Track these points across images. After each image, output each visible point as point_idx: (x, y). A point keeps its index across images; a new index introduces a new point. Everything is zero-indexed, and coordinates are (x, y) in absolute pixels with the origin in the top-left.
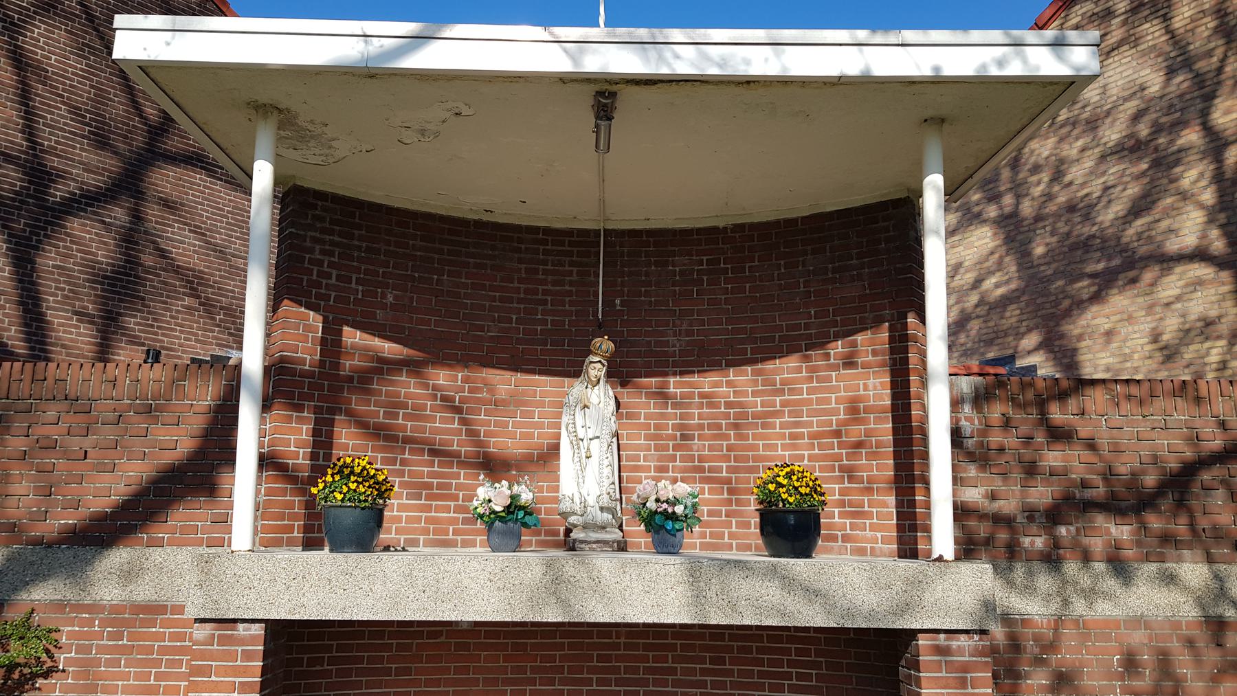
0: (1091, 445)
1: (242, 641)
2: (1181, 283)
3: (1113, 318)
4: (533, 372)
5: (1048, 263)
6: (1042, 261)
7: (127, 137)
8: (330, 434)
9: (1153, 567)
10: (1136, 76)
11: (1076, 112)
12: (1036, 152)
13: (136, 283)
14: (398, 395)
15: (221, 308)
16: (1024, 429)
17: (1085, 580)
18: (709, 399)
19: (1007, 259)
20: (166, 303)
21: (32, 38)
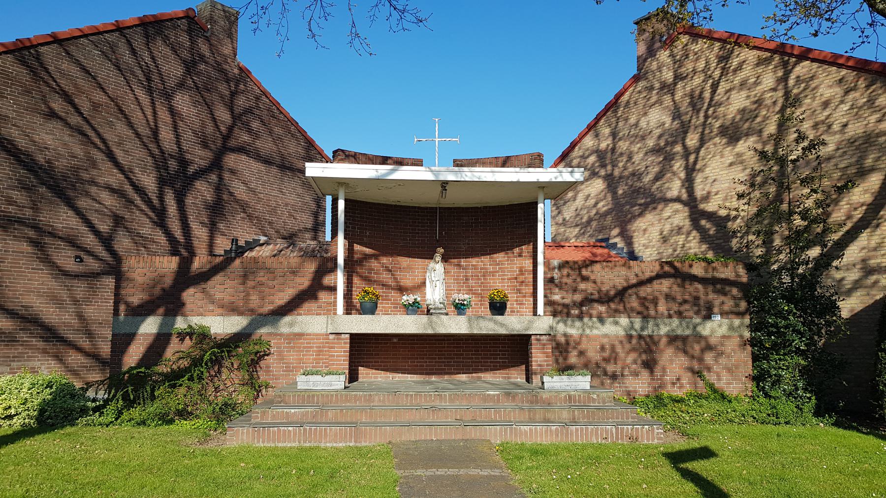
0: (595, 282)
1: (343, 339)
2: (671, 210)
3: (647, 224)
4: (415, 258)
5: (624, 198)
6: (622, 197)
7: (215, 142)
8: (352, 280)
9: (612, 319)
10: (660, 119)
11: (637, 131)
12: (621, 147)
13: (222, 208)
14: (371, 266)
15: (256, 217)
16: (574, 277)
17: (590, 324)
18: (475, 267)
19: (608, 194)
20: (234, 216)
21: (177, 101)
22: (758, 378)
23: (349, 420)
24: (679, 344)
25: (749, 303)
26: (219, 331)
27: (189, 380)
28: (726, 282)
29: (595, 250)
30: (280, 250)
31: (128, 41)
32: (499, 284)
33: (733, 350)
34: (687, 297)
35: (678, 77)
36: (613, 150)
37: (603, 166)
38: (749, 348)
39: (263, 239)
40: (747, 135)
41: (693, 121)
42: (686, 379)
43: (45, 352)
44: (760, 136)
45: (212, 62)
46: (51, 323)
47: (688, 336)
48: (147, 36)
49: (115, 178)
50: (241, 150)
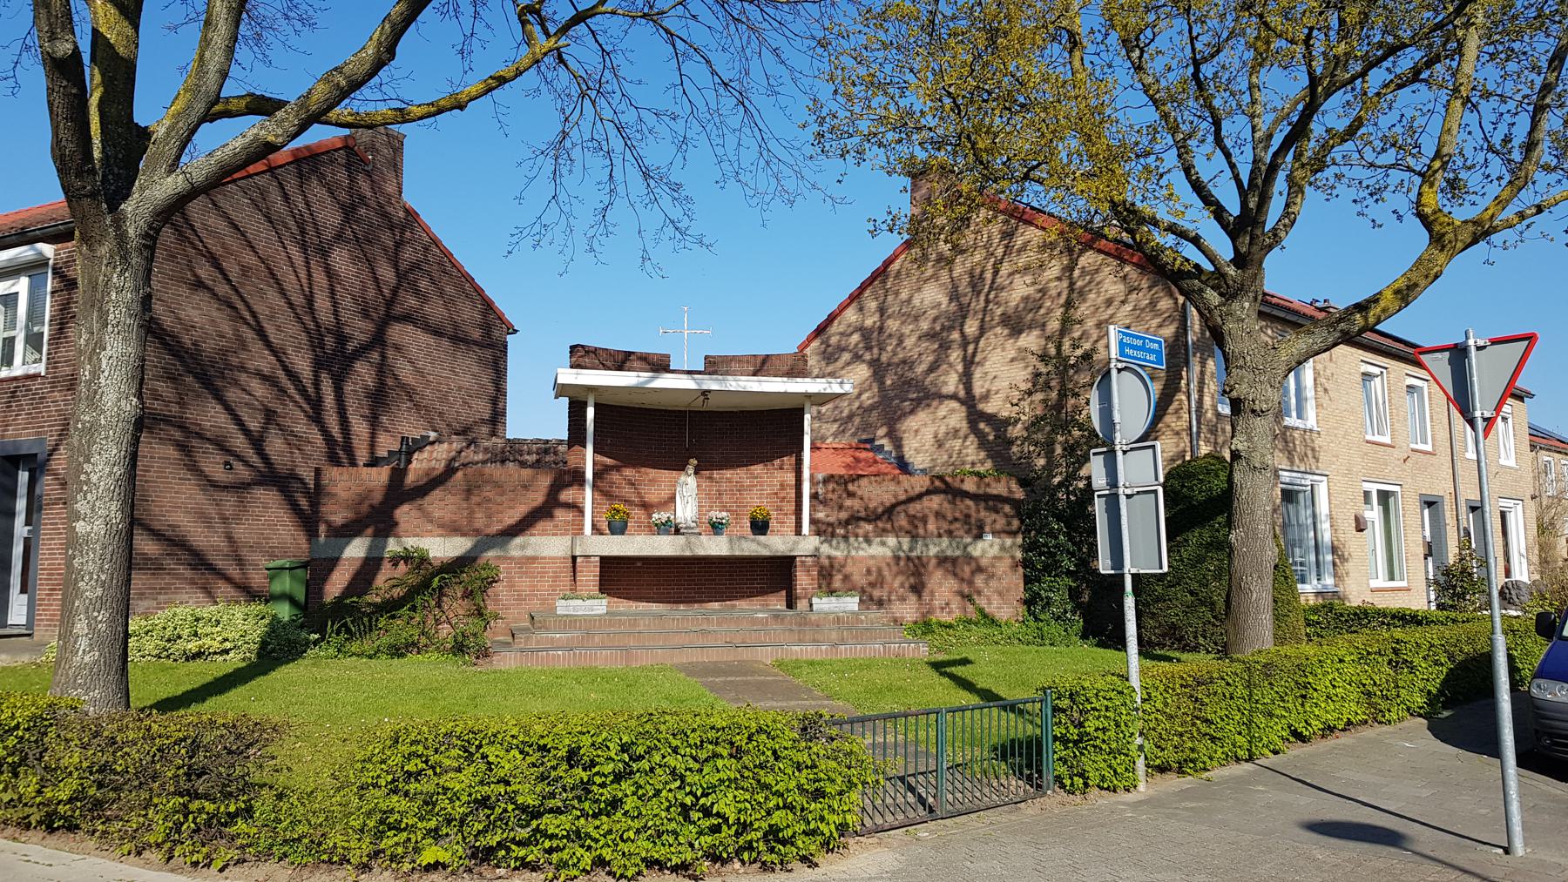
0: (862, 499)
9: (879, 539)
18: (729, 481)
22: (1029, 603)
23: (616, 644)
24: (949, 565)
25: (1022, 522)
26: (438, 555)
27: (409, 610)
28: (999, 498)
29: (857, 454)
30: (458, 450)
31: (279, 183)
32: (757, 501)
33: (1004, 572)
34: (957, 515)
35: (957, 249)
36: (881, 329)
37: (869, 348)
38: (1021, 570)
39: (433, 435)
40: (1030, 328)
41: (973, 305)
42: (956, 602)
43: (193, 583)
44: (1043, 330)
45: (374, 205)
46: (199, 546)
47: (958, 557)
48: (301, 176)
49: (263, 361)
50: (407, 318)
